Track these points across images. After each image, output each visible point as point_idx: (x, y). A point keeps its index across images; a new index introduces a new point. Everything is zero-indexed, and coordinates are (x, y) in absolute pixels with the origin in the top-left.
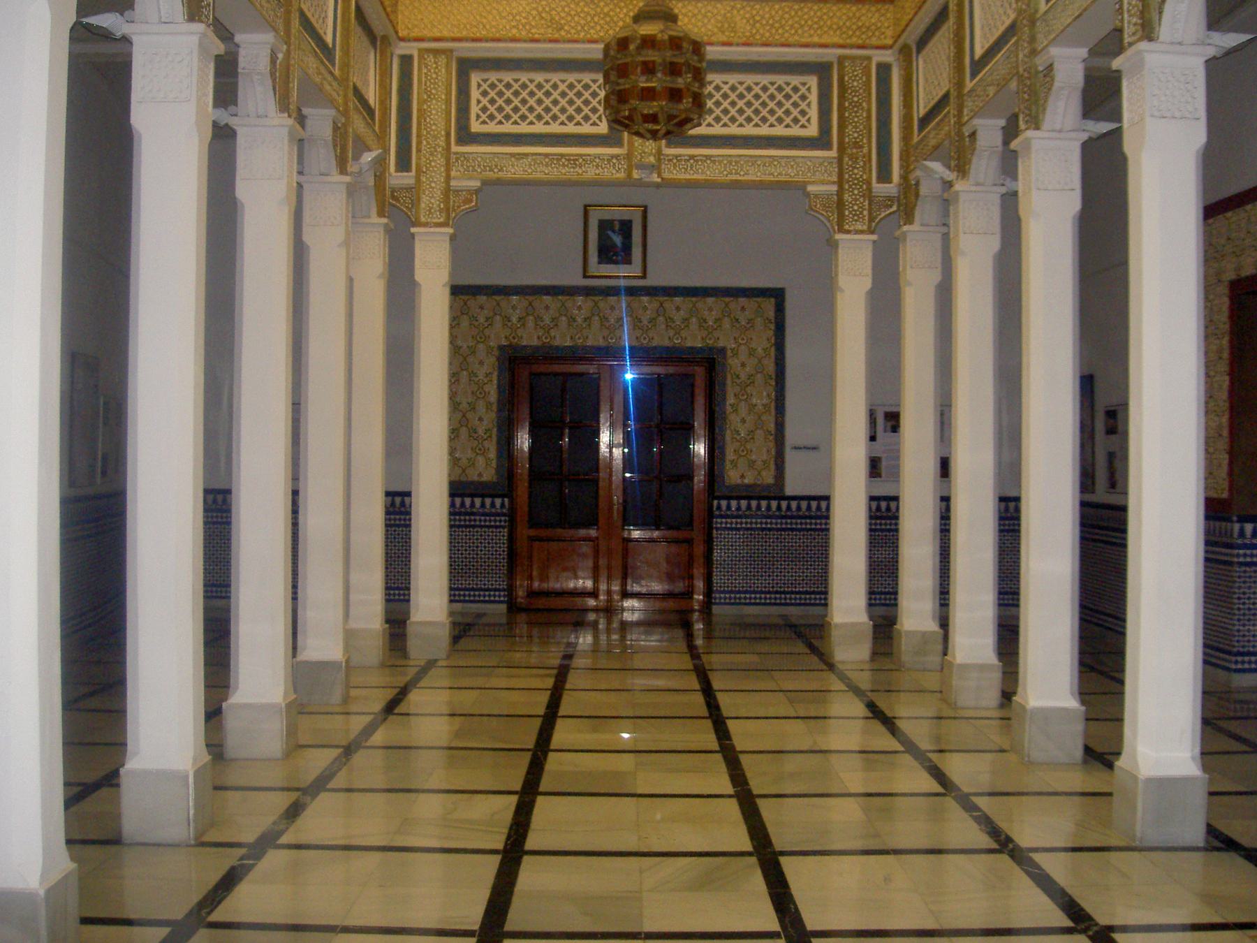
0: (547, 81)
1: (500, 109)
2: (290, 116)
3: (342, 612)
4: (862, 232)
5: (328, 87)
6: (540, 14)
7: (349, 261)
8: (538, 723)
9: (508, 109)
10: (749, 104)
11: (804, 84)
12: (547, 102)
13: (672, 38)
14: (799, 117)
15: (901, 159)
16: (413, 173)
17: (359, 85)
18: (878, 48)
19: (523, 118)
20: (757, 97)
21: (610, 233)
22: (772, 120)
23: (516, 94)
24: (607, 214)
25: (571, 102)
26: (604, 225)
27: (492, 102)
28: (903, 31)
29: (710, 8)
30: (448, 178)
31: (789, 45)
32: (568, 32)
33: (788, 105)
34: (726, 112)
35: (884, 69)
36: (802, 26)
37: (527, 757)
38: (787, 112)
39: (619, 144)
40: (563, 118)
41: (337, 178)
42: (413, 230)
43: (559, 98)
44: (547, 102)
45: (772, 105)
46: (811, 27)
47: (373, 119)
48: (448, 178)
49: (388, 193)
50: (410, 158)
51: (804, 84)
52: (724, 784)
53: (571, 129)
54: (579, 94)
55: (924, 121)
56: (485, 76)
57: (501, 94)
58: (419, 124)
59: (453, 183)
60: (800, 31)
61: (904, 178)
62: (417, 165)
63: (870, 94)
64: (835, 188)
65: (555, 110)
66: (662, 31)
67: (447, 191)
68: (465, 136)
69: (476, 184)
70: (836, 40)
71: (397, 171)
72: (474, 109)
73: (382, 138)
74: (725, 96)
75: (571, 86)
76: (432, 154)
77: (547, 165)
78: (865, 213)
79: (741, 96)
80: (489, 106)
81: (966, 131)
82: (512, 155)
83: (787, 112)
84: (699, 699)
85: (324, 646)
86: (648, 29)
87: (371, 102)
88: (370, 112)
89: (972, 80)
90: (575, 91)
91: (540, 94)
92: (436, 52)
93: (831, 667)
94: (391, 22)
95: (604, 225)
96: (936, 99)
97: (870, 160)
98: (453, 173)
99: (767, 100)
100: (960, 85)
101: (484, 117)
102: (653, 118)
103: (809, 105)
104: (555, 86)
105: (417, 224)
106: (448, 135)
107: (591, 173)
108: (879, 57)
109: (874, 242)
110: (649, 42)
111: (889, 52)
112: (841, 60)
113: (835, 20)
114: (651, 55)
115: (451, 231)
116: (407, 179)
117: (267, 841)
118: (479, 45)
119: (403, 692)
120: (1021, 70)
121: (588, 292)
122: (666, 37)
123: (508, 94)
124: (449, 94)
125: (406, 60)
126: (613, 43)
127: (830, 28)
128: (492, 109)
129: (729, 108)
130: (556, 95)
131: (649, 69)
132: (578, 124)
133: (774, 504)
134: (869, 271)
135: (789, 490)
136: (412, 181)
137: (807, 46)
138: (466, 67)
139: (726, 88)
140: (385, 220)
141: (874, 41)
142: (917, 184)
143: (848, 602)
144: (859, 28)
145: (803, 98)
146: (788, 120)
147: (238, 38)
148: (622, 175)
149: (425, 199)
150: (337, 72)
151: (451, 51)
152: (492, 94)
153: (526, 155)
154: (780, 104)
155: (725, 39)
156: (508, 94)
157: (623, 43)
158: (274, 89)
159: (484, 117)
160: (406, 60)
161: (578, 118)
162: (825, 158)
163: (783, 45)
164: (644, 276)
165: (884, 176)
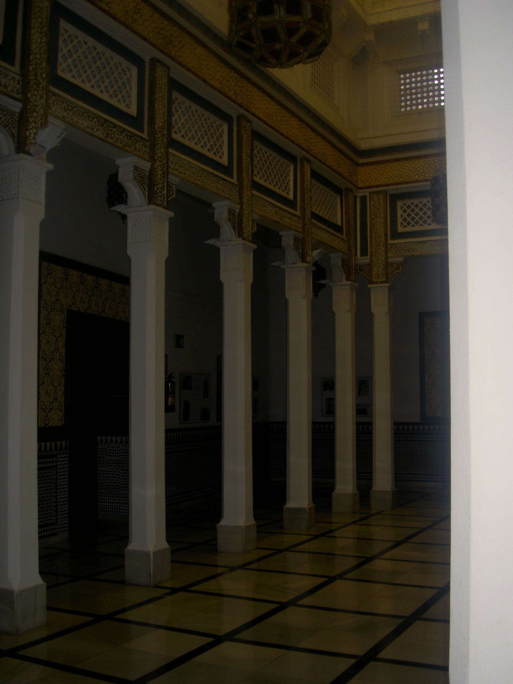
16: (369, 257)
23: (421, 210)
27: (409, 215)
30: (387, 258)
48: (387, 258)
56: (404, 202)
57: (413, 211)
58: (371, 231)
59: (389, 260)
67: (387, 264)
68: (396, 235)
71: (361, 256)
92: (378, 193)
98: (389, 255)
105: (371, 283)
106: (386, 235)
125: (363, 198)
138: (395, 198)
151: (386, 191)
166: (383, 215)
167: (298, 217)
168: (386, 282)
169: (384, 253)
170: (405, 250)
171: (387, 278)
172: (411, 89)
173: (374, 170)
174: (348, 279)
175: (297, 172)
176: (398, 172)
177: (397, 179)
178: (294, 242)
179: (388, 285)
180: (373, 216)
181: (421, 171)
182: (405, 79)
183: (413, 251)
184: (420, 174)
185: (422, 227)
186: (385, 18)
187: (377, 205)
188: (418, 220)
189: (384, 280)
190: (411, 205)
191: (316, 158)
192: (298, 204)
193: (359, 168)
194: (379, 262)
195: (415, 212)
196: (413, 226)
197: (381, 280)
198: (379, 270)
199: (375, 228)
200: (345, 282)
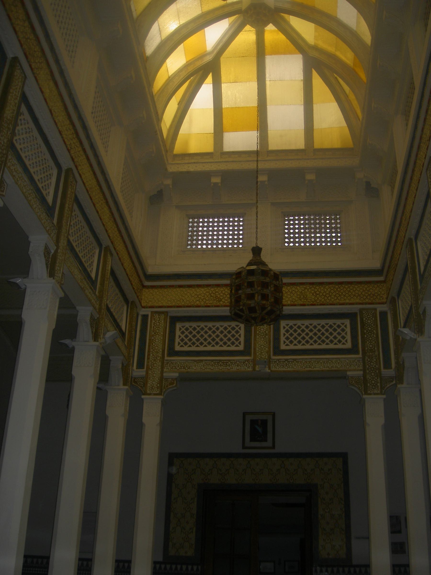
0: (214, 326)
1: (190, 340)
4: (377, 394)
6: (210, 294)
9: (194, 340)
10: (315, 334)
11: (343, 324)
16: (145, 369)
18: (380, 303)
21: (257, 427)
23: (198, 332)
24: (255, 417)
25: (225, 336)
26: (253, 422)
27: (186, 336)
29: (294, 289)
30: (162, 372)
31: (334, 304)
32: (224, 302)
33: (335, 334)
34: (303, 338)
35: (383, 315)
38: (335, 338)
40: (221, 343)
41: (92, 343)
44: (214, 336)
45: (327, 334)
46: (345, 296)
48: (162, 372)
50: (144, 362)
51: (343, 324)
56: (183, 324)
57: (191, 333)
58: (149, 346)
59: (164, 374)
63: (377, 326)
64: (362, 373)
65: (217, 340)
67: (162, 378)
68: (172, 352)
69: (177, 375)
70: (358, 301)
72: (177, 340)
74: (303, 331)
75: (226, 328)
76: (155, 360)
78: (379, 384)
79: (311, 331)
80: (185, 338)
81: (421, 311)
83: (335, 338)
87: (123, 328)
91: (210, 332)
92: (159, 313)
95: (253, 422)
97: (379, 358)
98: (165, 370)
99: (324, 332)
103: (346, 334)
104: (218, 329)
107: (235, 368)
108: (380, 308)
111: (385, 305)
112: (361, 310)
113: (357, 292)
114: (251, 279)
116: (141, 373)
118: (180, 309)
121: (245, 456)
123: (194, 333)
125: (145, 317)
127: (354, 295)
135: (355, 562)
136: (144, 373)
138: (174, 320)
142: (403, 363)
144: (369, 295)
145: (343, 330)
146: (336, 341)
148: (251, 369)
151: (167, 312)
152: (187, 333)
153: (202, 361)
155: (302, 303)
158: (47, 264)
160: (145, 317)
163: (331, 304)
164: (273, 447)
165: (387, 365)
166: (162, 333)
168: (160, 394)
171: (161, 390)
173: (158, 293)
174: (124, 384)
175: (101, 258)
176: (180, 297)
177: (178, 302)
178: (91, 318)
179: (161, 397)
180: (153, 333)
181: (202, 298)
183: (188, 368)
184: (201, 300)
187: (158, 324)
189: (158, 392)
190: (189, 328)
191: (117, 254)
193: (144, 289)
197: (155, 392)
199: (154, 344)
200: (122, 387)
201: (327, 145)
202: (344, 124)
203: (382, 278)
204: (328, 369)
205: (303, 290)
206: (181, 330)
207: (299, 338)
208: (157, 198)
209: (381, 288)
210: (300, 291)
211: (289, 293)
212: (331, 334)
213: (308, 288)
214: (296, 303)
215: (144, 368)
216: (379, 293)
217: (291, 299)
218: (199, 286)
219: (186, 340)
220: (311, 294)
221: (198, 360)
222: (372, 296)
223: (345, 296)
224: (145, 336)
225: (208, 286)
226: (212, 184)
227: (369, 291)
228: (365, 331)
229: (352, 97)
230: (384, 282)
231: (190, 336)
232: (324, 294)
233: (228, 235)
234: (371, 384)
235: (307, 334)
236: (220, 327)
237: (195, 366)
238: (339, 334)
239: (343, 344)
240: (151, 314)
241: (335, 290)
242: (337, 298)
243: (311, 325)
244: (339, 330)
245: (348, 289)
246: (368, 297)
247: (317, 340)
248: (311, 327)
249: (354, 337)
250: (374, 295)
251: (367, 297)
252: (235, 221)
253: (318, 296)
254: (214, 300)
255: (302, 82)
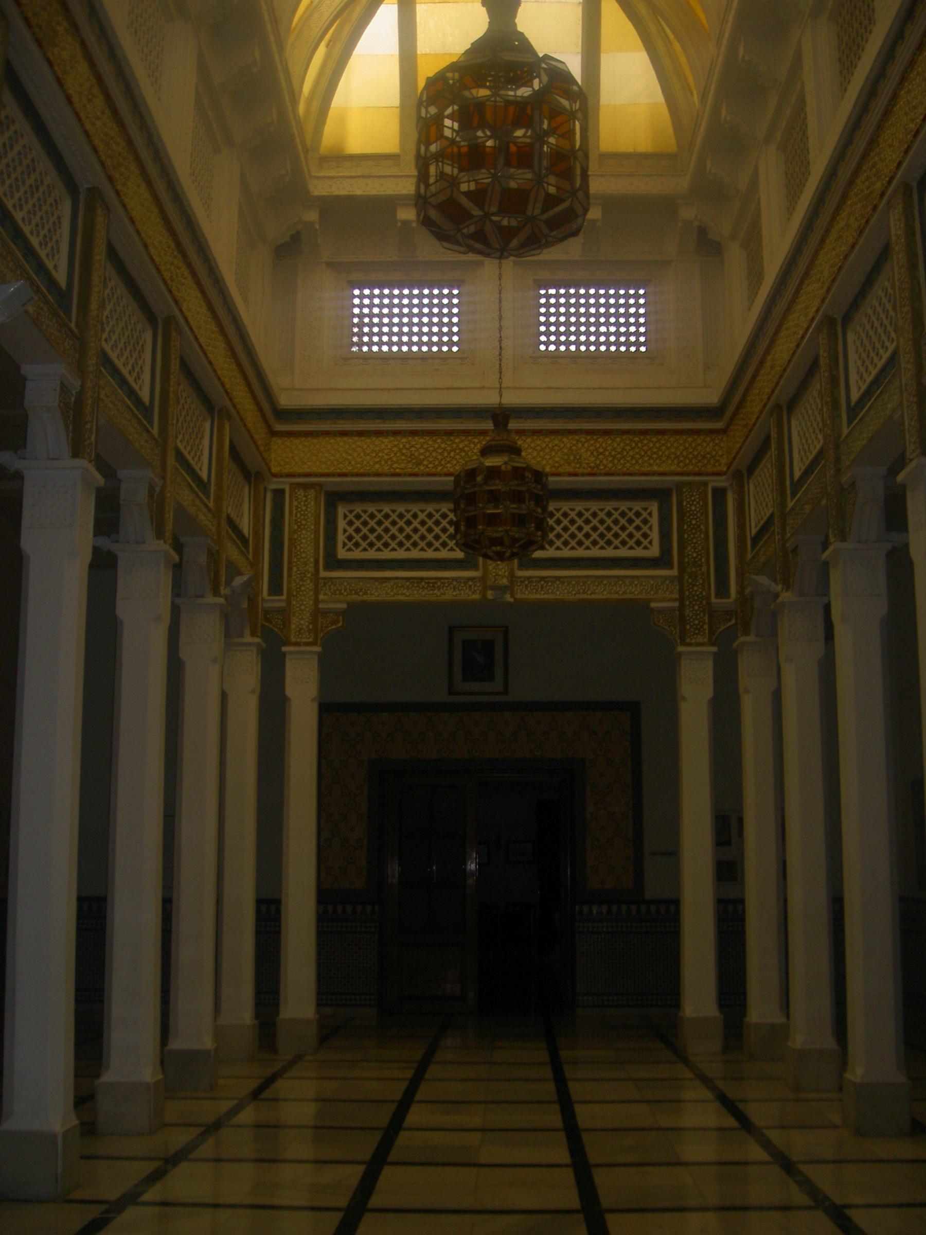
0: (408, 511)
2: (165, 542)
3: (215, 1010)
4: (703, 644)
5: (202, 517)
7: (225, 678)
8: (393, 1107)
9: (372, 537)
10: (595, 529)
11: (645, 509)
12: (408, 530)
13: (515, 469)
14: (642, 539)
15: (737, 575)
16: (284, 597)
17: (233, 516)
19: (386, 545)
20: (602, 522)
22: (616, 542)
23: (380, 523)
25: (430, 530)
28: (734, 458)
29: (556, 442)
30: (317, 601)
31: (630, 474)
33: (631, 528)
36: (642, 457)
37: (379, 1135)
38: (631, 536)
39: (475, 567)
40: (423, 544)
41: (211, 599)
42: (284, 649)
43: (419, 526)
45: (616, 529)
47: (247, 547)
48: (317, 601)
49: (260, 615)
50: (282, 582)
52: (564, 1156)
53: (430, 554)
54: (437, 523)
55: (756, 540)
56: (351, 507)
57: (365, 524)
58: (290, 551)
60: (640, 462)
61: (741, 592)
62: (289, 590)
64: (676, 604)
65: (416, 537)
66: (506, 463)
68: (333, 562)
69: (344, 606)
71: (269, 595)
72: (341, 538)
73: (255, 564)
74: (572, 522)
76: (302, 580)
77: (408, 588)
78: (706, 627)
79: (587, 522)
82: (376, 579)
84: (551, 1086)
85: (195, 1032)
86: (492, 461)
87: (246, 531)
88: (245, 541)
89: (792, 500)
90: (434, 519)
91: (401, 523)
92: (305, 487)
93: (685, 1060)
94: (263, 459)
96: (765, 518)
97: (709, 577)
98: (321, 597)
99: (612, 525)
100: (782, 504)
101: (350, 545)
102: (498, 542)
103: (650, 528)
105: (288, 643)
106: (317, 562)
107: (449, 595)
108: (715, 482)
109: (715, 653)
110: (493, 473)
111: (723, 478)
112: (679, 486)
114: (497, 485)
115: (318, 649)
117: (130, 1198)
119: (271, 1080)
120: (829, 488)
122: (509, 468)
123: (372, 523)
124: (317, 523)
126: (462, 474)
127: (668, 457)
128: (357, 538)
129: (576, 532)
130: (416, 523)
131: (494, 498)
132: (437, 549)
133: (634, 908)
134: (710, 680)
137: (647, 474)
138: (334, 498)
139: (573, 515)
140: (257, 640)
141: (709, 469)
143: (699, 998)
144: (695, 457)
145: (645, 522)
146: (631, 543)
147: (121, 474)
148: (477, 596)
149: (295, 621)
150: (211, 505)
151: (320, 485)
152: (358, 524)
153: (389, 579)
154: (623, 528)
156: (372, 523)
157: (471, 474)
159: (350, 545)
160: (279, 494)
161: (437, 544)
162: (666, 578)
163: (625, 474)
164: (506, 692)
165: (722, 589)
167: (209, 510)
169: (312, 593)
170: (351, 591)
172: (371, 316)
180: (296, 527)
181: (386, 457)
182: (362, 297)
184: (383, 463)
185: (380, 553)
186: (341, 189)
187: (304, 508)
188: (374, 540)
189: (311, 640)
192: (212, 491)
193: (274, 439)
194: (303, 607)
195: (369, 526)
196: (365, 550)
198: (302, 622)
200: (248, 639)
201: (625, 146)
202: (659, 98)
203: (719, 425)
204: (616, 596)
205: (574, 445)
206: (348, 519)
207: (566, 536)
208: (290, 251)
209: (717, 444)
210: (568, 445)
211: (547, 450)
212: (623, 528)
213: (583, 440)
214: (561, 470)
215: (282, 594)
216: (714, 453)
217: (550, 462)
218: (379, 433)
219: (357, 538)
220: (589, 453)
221: (382, 578)
222: (700, 458)
223: (650, 457)
224: (281, 532)
225: (396, 433)
226: (399, 224)
227: (694, 448)
228: (685, 527)
229: (683, 59)
230: (724, 431)
231: (365, 530)
232: (613, 453)
233: (430, 324)
234: (691, 627)
235: (580, 529)
236: (419, 513)
237: (377, 589)
238: (638, 528)
239: (646, 548)
240: (290, 488)
241: (634, 445)
242: (637, 461)
243: (587, 510)
244: (638, 522)
245: (657, 445)
246: (694, 461)
247: (598, 539)
248: (587, 515)
249: (665, 536)
250: (704, 457)
251: (690, 461)
252: (444, 296)
253: (601, 457)
254: (409, 462)
255: (580, 8)
